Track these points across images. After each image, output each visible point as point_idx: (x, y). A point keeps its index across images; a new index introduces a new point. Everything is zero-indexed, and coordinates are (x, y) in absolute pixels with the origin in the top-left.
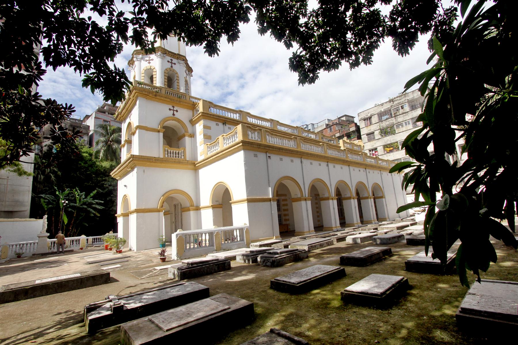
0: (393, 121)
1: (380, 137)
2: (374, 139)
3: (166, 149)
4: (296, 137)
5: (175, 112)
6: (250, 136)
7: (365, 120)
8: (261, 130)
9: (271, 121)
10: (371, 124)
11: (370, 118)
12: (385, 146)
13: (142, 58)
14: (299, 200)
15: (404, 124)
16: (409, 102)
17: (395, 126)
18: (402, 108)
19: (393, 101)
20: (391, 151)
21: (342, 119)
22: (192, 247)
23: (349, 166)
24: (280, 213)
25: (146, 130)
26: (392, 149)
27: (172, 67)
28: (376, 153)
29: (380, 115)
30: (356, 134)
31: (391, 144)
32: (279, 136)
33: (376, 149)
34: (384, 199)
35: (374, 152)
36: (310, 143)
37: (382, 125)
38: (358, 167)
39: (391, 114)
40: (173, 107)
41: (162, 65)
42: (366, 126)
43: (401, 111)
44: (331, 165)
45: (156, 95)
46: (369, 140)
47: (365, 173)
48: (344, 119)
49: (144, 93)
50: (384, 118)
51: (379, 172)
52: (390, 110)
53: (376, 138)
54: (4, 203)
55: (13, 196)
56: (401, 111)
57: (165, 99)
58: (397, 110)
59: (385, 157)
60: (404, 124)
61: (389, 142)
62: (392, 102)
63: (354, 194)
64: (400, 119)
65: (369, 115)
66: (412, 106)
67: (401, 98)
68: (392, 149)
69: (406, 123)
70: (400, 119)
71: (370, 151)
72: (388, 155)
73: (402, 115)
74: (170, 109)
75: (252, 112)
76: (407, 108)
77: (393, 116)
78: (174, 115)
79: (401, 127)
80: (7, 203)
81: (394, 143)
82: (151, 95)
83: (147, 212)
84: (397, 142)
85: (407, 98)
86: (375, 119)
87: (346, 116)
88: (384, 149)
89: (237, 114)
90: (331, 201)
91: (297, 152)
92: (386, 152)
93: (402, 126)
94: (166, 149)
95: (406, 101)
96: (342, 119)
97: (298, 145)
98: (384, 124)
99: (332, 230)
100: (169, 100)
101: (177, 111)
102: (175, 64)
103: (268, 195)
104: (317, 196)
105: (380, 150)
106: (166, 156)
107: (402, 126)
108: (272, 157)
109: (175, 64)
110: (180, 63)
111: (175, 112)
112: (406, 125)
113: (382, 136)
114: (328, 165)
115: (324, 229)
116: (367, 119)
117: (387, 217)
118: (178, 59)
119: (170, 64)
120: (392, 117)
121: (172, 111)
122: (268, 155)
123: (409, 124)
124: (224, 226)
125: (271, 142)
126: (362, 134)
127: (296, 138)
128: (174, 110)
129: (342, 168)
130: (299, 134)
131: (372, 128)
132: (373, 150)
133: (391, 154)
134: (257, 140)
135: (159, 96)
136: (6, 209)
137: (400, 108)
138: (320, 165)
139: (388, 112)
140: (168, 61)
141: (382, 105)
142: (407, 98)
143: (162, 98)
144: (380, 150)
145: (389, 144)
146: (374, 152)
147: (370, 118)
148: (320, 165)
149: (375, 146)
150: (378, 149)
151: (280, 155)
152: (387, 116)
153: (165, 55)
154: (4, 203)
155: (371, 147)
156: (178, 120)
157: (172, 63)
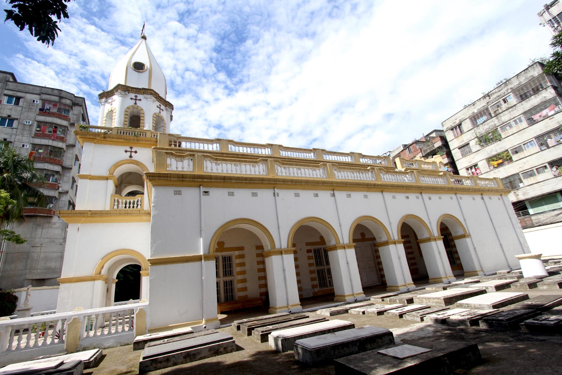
0: (494, 122)
1: (478, 147)
2: (470, 152)
3: (116, 199)
4: (373, 168)
5: (133, 154)
6: (336, 175)
7: (452, 129)
8: (193, 155)
9: (352, 154)
10: (462, 132)
11: (460, 125)
12: (490, 160)
13: (106, 102)
14: (428, 240)
15: (513, 123)
16: (514, 91)
17: (499, 129)
18: (505, 101)
19: (489, 96)
20: (500, 165)
21: (431, 135)
22: (113, 331)
23: (382, 192)
24: (328, 267)
25: (90, 179)
26: (500, 161)
27: (136, 104)
28: (478, 171)
29: (474, 119)
30: (445, 150)
31: (499, 154)
32: (249, 162)
33: (476, 165)
34: (468, 240)
35: (473, 170)
36: (297, 165)
37: (478, 131)
38: (294, 189)
39: (490, 114)
40: (131, 148)
41: (122, 103)
42: (456, 137)
43: (504, 106)
44: (486, 197)
45: (105, 138)
46: (464, 155)
47: (501, 200)
48: (434, 135)
49: (88, 136)
50: (479, 121)
51: (419, 195)
52: (487, 109)
53: (473, 150)
54: (35, 271)
55: (45, 263)
56: (504, 106)
57: (117, 140)
58: (498, 106)
59: (491, 175)
60: (513, 123)
61: (494, 153)
62: (487, 98)
63: (436, 232)
64: (505, 117)
65: (457, 122)
66: (521, 96)
67: (499, 89)
68: (500, 161)
69: (515, 121)
70: (505, 117)
71: (467, 169)
72: (497, 170)
73: (506, 112)
74: (126, 151)
75: (328, 148)
76: (513, 100)
77: (493, 115)
78: (131, 157)
79: (508, 128)
80: (39, 271)
81: (503, 153)
82: (98, 138)
83: (77, 281)
84: (507, 150)
85: (510, 86)
86: (467, 125)
87: (435, 131)
88: (488, 164)
89: (349, 157)
90: (433, 243)
91: (269, 180)
92: (492, 168)
93: (511, 127)
94: (116, 199)
95: (509, 91)
96: (431, 135)
97: (270, 170)
98: (482, 130)
99: (398, 290)
100: (123, 140)
101: (136, 152)
102: (140, 100)
103: (198, 250)
104: (366, 239)
105: (483, 166)
106: (116, 207)
107: (511, 127)
108: (396, 197)
109: (140, 100)
110: (147, 98)
111: (133, 154)
112: (516, 123)
113: (482, 146)
114: (483, 198)
115: (335, 298)
116: (456, 127)
117: (477, 268)
118: (144, 93)
119: (138, 98)
120: (492, 118)
121: (129, 154)
122: (203, 189)
123: (521, 121)
124: (106, 306)
125: (386, 180)
126: (451, 148)
127: (413, 172)
128: (131, 152)
129: (440, 198)
130: (356, 163)
131: (464, 138)
132: (471, 168)
133: (501, 168)
134: (263, 175)
135: (109, 137)
136: (38, 277)
137: (502, 102)
138: (474, 199)
139: (485, 112)
140: (132, 99)
141: (474, 104)
142: (510, 86)
143: (114, 140)
144: (483, 166)
145: (495, 156)
146: (473, 170)
147: (460, 125)
148: (474, 199)
149: (473, 162)
150: (480, 165)
151: (229, 187)
152: (485, 118)
153: (127, 93)
154: (35, 271)
155: (468, 165)
156: (137, 163)
157: (136, 100)
